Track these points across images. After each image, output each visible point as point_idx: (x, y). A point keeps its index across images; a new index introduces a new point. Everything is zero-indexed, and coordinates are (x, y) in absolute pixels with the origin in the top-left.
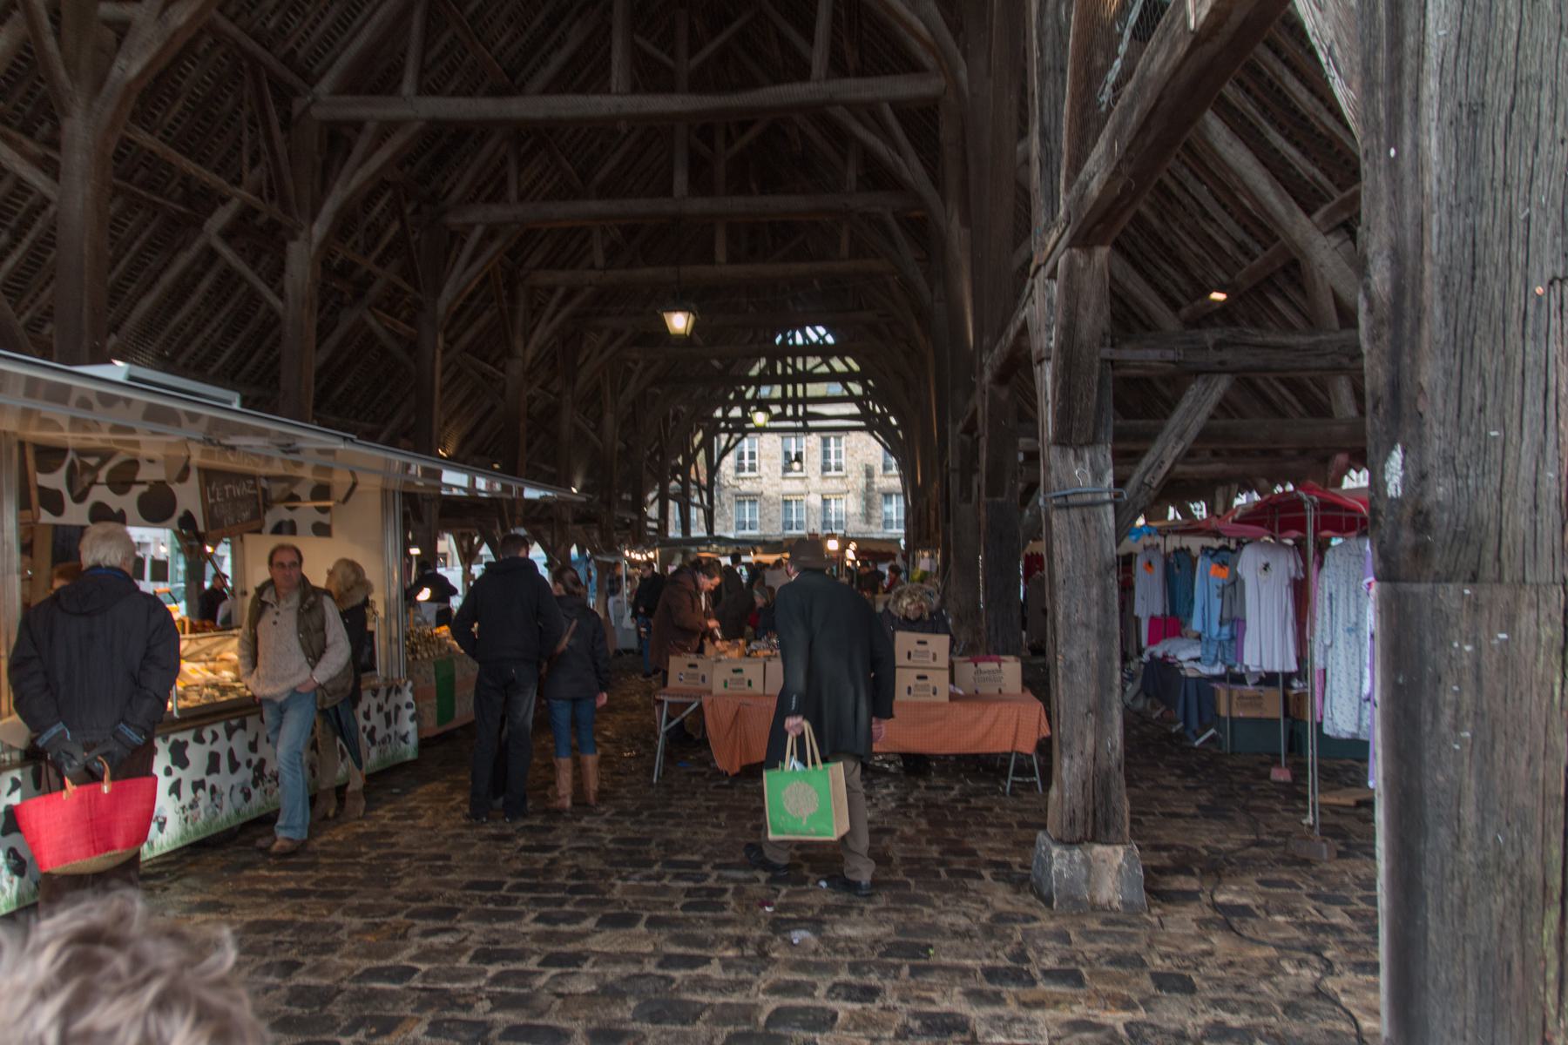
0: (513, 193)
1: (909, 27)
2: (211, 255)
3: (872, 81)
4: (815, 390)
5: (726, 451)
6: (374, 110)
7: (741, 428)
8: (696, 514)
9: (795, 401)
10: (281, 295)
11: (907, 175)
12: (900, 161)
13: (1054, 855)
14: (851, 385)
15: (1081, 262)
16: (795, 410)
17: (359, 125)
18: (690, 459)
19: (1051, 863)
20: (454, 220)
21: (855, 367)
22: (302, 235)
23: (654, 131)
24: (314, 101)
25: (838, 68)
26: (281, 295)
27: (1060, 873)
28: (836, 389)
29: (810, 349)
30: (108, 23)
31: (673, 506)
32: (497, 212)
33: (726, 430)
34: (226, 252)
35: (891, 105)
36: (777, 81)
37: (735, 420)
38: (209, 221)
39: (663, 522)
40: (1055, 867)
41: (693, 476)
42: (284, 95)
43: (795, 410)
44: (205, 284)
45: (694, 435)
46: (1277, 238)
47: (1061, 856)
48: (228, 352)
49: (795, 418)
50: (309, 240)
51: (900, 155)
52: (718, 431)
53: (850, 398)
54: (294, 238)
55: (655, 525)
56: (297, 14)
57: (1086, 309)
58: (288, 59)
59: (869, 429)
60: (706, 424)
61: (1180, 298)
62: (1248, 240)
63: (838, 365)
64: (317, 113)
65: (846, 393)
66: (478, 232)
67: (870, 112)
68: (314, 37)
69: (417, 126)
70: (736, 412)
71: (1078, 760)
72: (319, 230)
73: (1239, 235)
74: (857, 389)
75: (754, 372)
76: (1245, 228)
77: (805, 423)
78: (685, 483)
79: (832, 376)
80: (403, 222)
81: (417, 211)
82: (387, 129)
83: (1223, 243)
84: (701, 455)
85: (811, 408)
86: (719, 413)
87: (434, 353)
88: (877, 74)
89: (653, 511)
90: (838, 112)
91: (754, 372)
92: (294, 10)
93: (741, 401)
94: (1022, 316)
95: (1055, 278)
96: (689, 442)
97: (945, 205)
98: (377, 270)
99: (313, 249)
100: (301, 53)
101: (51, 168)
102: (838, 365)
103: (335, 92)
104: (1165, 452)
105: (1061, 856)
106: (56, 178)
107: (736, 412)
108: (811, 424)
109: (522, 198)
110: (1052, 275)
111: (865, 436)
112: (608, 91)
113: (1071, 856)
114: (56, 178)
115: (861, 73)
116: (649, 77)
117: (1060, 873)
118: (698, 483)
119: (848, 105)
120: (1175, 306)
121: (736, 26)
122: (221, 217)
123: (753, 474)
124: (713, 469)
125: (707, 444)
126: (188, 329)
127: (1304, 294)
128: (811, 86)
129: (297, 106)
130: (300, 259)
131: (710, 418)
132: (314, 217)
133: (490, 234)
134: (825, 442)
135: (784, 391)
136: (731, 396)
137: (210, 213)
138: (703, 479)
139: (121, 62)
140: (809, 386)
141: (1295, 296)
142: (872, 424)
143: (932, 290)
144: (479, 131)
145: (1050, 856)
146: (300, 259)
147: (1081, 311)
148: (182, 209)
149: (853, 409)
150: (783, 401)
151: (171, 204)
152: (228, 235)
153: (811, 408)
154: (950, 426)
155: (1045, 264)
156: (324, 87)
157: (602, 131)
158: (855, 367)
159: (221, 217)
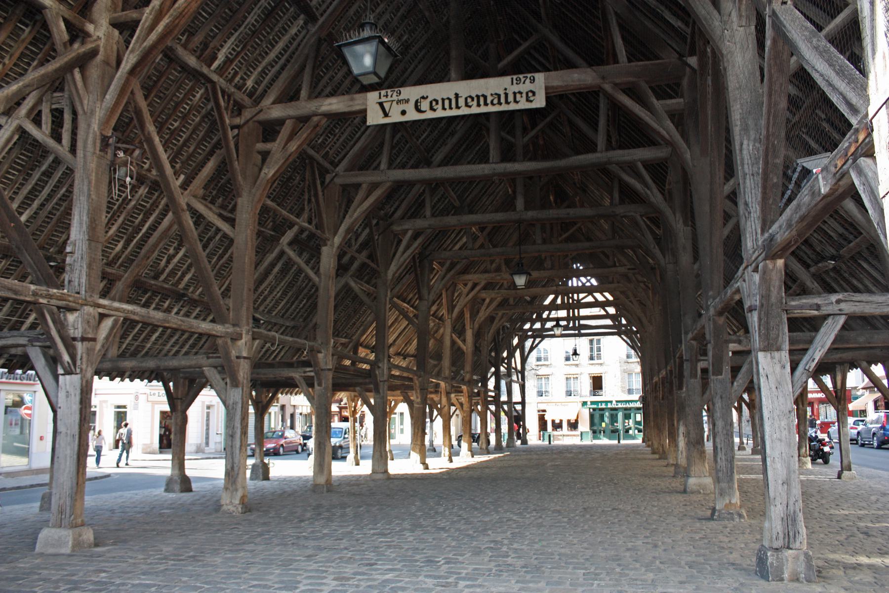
0: (428, 213)
1: (659, 133)
2: (282, 253)
3: (632, 151)
4: (584, 312)
5: (532, 349)
6: (366, 178)
7: (541, 335)
8: (516, 388)
9: (574, 318)
10: (317, 273)
11: (653, 199)
12: (649, 192)
13: (769, 555)
14: (607, 308)
15: (770, 266)
16: (574, 323)
17: (358, 186)
18: (511, 355)
19: (767, 559)
20: (396, 228)
21: (611, 298)
22: (329, 243)
23: (512, 178)
24: (336, 175)
25: (610, 147)
26: (317, 273)
27: (772, 563)
28: (597, 311)
29: (583, 289)
30: (259, 152)
31: (503, 383)
32: (420, 223)
33: (531, 337)
34: (291, 253)
35: (641, 162)
36: (578, 153)
37: (536, 329)
38: (283, 238)
39: (497, 392)
40: (770, 560)
41: (513, 365)
42: (323, 172)
43: (574, 323)
44: (276, 269)
45: (513, 340)
46: (861, 234)
47: (773, 555)
48: (283, 303)
49: (574, 328)
50: (332, 245)
51: (648, 189)
52: (527, 337)
53: (607, 316)
54: (326, 245)
55: (493, 394)
56: (332, 134)
57: (774, 287)
58: (326, 156)
59: (619, 334)
60: (521, 333)
61: (809, 261)
62: (845, 232)
63: (600, 297)
64: (338, 181)
65: (604, 313)
66: (410, 233)
67: (630, 168)
68: (338, 145)
69: (388, 184)
70: (538, 325)
71: (779, 506)
72: (337, 240)
73: (841, 230)
74: (612, 310)
75: (547, 302)
76: (843, 226)
77: (579, 331)
78: (509, 368)
79: (596, 304)
80: (371, 229)
81: (377, 224)
82: (374, 186)
83: (832, 234)
84: (518, 354)
85: (582, 322)
86: (527, 326)
87: (386, 300)
88: (634, 148)
89: (491, 384)
90: (614, 168)
91: (547, 302)
92: (330, 132)
93: (539, 318)
94: (736, 286)
95: (757, 272)
96: (511, 343)
97: (675, 215)
98: (357, 255)
99: (335, 250)
100: (331, 152)
101: (232, 222)
102: (600, 297)
103: (346, 171)
104: (817, 353)
105: (773, 555)
106: (233, 226)
107: (538, 325)
108: (583, 331)
109: (433, 215)
110: (756, 270)
111: (616, 337)
112: (489, 163)
113: (777, 555)
114: (233, 226)
115: (620, 147)
116: (507, 155)
117: (772, 563)
118: (516, 369)
119: (618, 164)
120: (807, 266)
121: (548, 119)
122: (290, 235)
123: (546, 363)
124: (524, 360)
125: (521, 345)
126: (266, 292)
127: (879, 261)
128: (598, 155)
129: (328, 178)
130: (328, 257)
131: (521, 329)
132: (335, 234)
133: (415, 237)
134: (591, 341)
135: (568, 313)
136: (534, 317)
137: (283, 234)
138: (519, 367)
139: (265, 170)
140: (581, 310)
141: (874, 262)
142: (618, 330)
143: (664, 257)
144: (411, 184)
145: (766, 555)
146: (328, 257)
147: (772, 289)
148: (272, 233)
149: (608, 322)
150: (567, 319)
151: (267, 231)
152: (290, 244)
153: (582, 322)
154: (683, 336)
155: (751, 265)
156: (341, 168)
157: (486, 181)
158: (611, 298)
159: (290, 235)
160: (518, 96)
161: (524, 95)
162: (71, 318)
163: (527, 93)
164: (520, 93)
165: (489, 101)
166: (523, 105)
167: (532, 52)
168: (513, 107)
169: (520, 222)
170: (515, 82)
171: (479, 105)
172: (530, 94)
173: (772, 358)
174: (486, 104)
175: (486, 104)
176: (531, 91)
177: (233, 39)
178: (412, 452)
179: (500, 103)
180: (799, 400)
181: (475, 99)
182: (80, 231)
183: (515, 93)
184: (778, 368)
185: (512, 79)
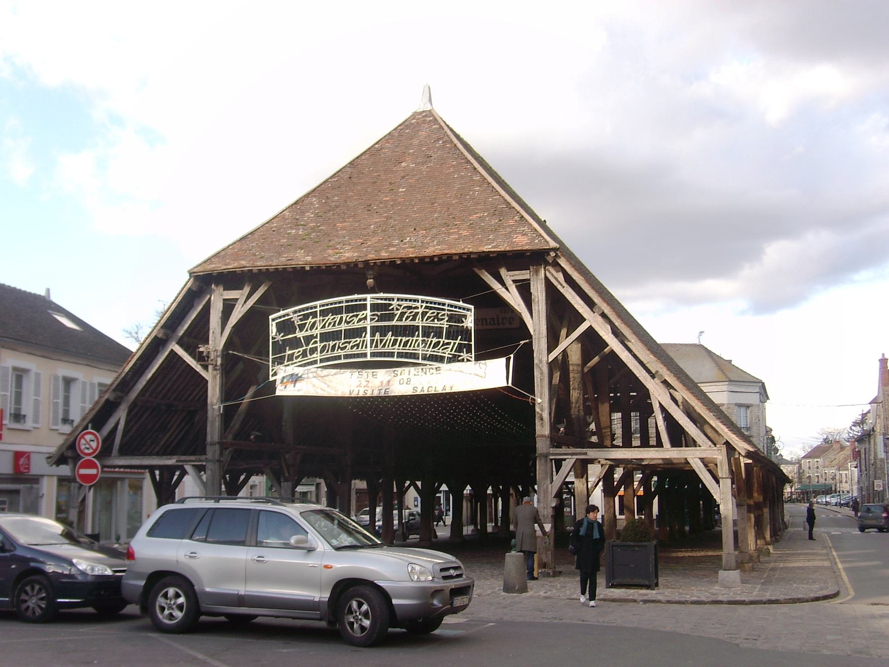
2: (365, 300)
160: (504, 320)
161: (508, 320)
162: (287, 456)
163: (510, 319)
164: (505, 318)
165: (488, 322)
166: (507, 326)
167: (653, 441)
168: (501, 326)
169: (453, 340)
170: (503, 311)
171: (482, 325)
172: (511, 320)
173: (580, 481)
174: (487, 324)
175: (487, 324)
176: (512, 318)
177: (791, 565)
178: (831, 565)
179: (494, 324)
180: (207, 518)
181: (481, 320)
182: (818, 571)
183: (503, 319)
184: (581, 485)
185: (501, 309)
